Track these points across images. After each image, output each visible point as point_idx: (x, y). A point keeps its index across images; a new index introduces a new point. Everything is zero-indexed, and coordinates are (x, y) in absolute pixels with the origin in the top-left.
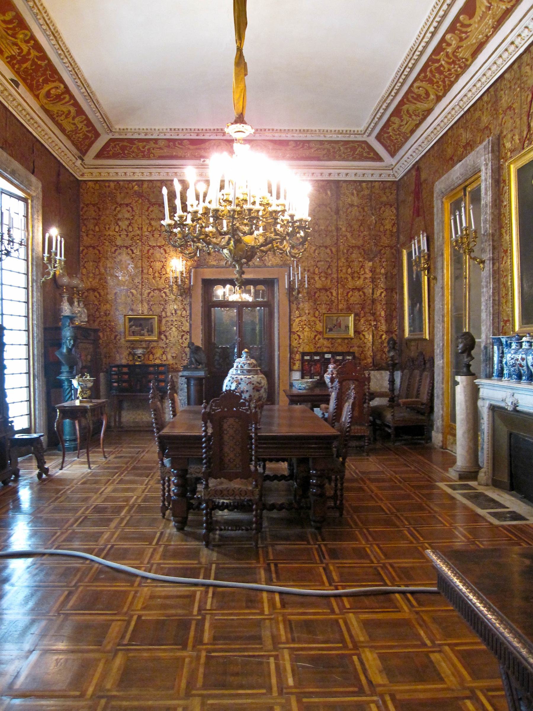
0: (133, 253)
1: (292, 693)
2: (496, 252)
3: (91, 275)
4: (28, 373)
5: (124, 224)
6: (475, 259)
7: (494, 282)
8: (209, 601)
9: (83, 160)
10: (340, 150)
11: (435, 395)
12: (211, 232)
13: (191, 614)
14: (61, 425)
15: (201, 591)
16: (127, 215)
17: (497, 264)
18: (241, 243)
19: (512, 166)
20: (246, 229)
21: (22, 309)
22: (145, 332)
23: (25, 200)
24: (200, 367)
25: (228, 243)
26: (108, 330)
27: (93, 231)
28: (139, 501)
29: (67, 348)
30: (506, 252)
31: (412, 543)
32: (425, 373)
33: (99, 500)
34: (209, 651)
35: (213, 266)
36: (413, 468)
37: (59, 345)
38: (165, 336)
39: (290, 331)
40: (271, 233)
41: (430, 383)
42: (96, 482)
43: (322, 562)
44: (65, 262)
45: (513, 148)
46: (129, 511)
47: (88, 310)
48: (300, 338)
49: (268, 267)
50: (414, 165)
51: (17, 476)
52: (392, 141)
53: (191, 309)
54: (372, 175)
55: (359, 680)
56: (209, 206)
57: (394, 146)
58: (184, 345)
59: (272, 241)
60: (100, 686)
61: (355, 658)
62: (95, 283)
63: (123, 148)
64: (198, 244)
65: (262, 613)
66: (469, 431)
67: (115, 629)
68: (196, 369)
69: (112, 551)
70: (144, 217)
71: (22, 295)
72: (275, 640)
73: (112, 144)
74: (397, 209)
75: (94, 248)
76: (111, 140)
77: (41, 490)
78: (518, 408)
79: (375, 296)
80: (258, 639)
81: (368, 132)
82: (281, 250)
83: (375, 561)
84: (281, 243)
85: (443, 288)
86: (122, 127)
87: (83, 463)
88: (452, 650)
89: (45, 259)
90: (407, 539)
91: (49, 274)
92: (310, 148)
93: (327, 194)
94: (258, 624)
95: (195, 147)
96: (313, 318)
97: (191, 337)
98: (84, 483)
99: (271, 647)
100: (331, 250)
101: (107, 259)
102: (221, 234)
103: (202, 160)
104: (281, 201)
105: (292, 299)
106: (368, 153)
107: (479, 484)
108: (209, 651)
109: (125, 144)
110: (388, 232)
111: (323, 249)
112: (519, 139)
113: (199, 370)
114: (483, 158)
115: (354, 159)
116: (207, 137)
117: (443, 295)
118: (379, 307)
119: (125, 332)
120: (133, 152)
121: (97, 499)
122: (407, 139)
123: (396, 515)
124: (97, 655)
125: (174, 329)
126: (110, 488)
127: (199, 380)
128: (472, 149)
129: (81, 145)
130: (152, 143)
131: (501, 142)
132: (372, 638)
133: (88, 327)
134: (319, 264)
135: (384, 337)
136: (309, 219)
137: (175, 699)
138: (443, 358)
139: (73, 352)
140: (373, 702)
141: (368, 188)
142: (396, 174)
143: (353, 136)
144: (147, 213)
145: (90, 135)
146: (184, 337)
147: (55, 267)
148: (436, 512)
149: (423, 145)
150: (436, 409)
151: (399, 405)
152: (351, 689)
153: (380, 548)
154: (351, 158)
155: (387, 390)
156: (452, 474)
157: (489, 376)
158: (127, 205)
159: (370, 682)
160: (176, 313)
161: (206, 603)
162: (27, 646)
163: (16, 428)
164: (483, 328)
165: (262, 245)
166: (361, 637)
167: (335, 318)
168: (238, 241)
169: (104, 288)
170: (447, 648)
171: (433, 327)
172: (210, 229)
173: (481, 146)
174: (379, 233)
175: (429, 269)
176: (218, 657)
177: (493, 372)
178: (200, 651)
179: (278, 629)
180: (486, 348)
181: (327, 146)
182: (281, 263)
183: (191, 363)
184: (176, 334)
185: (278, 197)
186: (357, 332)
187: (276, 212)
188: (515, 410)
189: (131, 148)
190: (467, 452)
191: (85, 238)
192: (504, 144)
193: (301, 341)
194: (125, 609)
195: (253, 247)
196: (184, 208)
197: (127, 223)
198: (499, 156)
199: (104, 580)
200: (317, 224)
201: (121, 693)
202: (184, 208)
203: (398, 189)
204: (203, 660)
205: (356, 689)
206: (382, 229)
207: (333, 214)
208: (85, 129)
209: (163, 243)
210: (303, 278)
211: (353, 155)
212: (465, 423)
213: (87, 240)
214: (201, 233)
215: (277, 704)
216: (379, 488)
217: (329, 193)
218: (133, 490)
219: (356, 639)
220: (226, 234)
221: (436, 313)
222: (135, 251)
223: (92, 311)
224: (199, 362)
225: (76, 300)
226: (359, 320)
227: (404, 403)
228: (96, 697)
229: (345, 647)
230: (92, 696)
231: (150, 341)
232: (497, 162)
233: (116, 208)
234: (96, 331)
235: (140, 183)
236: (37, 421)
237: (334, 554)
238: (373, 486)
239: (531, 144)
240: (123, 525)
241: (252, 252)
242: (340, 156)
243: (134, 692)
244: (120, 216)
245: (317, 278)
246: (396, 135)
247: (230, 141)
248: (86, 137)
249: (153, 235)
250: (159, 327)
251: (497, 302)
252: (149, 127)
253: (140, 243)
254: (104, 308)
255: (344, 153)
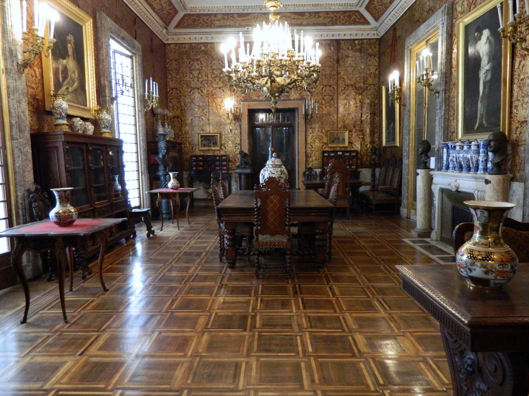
0: (202, 92)
1: (312, 356)
2: (447, 85)
3: (176, 107)
4: (138, 171)
5: (195, 73)
6: (432, 90)
7: (445, 106)
8: (259, 305)
9: (167, 29)
10: (340, 17)
11: (403, 183)
12: (256, 76)
13: (248, 312)
14: (160, 204)
15: (254, 299)
16: (198, 67)
17: (448, 94)
18: (275, 82)
19: (461, 24)
20: (278, 73)
21: (132, 129)
22: (212, 144)
23: (131, 57)
24: (247, 166)
25: (266, 83)
26: (187, 143)
27: (176, 78)
28: (212, 249)
29: (162, 155)
30: (454, 84)
31: (386, 274)
32: (396, 169)
33: (187, 248)
34: (260, 332)
35: (255, 100)
36: (387, 230)
37: (157, 153)
38: (224, 147)
39: (306, 143)
40: (295, 75)
41: (399, 175)
42: (184, 238)
43: (328, 284)
44: (159, 98)
45: (462, 11)
46: (206, 255)
47: (174, 130)
48: (312, 147)
49: (291, 100)
50: (392, 27)
51: (135, 236)
52: (377, 10)
53: (241, 129)
54: (362, 35)
55: (353, 349)
56: (254, 58)
57: (378, 13)
58: (236, 153)
59: (296, 81)
60: (196, 351)
61: (350, 338)
62: (178, 113)
63: (194, 20)
64: (247, 84)
65: (291, 312)
66: (425, 205)
67: (202, 321)
68: (245, 168)
69: (197, 278)
70: (209, 68)
71: (132, 120)
72: (300, 326)
73: (186, 18)
74: (379, 58)
75: (176, 89)
76: (185, 15)
77: (149, 244)
78: (459, 190)
79: (363, 118)
80: (290, 326)
81: (360, 4)
82: (301, 87)
83: (362, 284)
84: (301, 82)
85: (409, 111)
86: (192, 6)
87: (175, 227)
88: (412, 336)
89: (146, 96)
90: (383, 272)
91: (149, 106)
92: (319, 17)
93: (331, 49)
94: (290, 317)
95: (241, 19)
96: (322, 134)
97: (241, 148)
98: (176, 239)
99: (297, 330)
100: (333, 88)
101: (186, 97)
102: (262, 77)
103: (247, 28)
104: (302, 53)
105: (307, 121)
106: (360, 19)
107: (432, 240)
108: (260, 332)
109: (195, 17)
110: (372, 75)
111: (328, 87)
112: (467, 4)
113: (248, 168)
114: (441, 19)
115: (350, 24)
116: (249, 11)
117: (409, 116)
118: (365, 126)
119: (198, 145)
120: (200, 23)
121: (185, 248)
122: (387, 8)
123: (376, 258)
124: (192, 334)
125: (230, 142)
126: (193, 242)
127: (247, 175)
128: (433, 13)
129: (166, 19)
130: (213, 16)
131: (454, 6)
132: (361, 326)
133: (174, 141)
134: (326, 98)
135: (368, 146)
136: (320, 65)
137: (241, 358)
138: (409, 159)
139: (166, 157)
140: (361, 362)
141: (359, 44)
142: (379, 34)
143: (349, 7)
144: (210, 65)
145: (171, 12)
146: (237, 148)
147: (152, 102)
148: (402, 256)
149: (398, 12)
150: (403, 192)
151: (377, 190)
152: (348, 354)
153: (366, 277)
154: (347, 23)
155: (370, 181)
156: (414, 233)
157: (440, 169)
158: (197, 60)
159: (359, 351)
160: (231, 132)
161: (257, 306)
162: (150, 329)
163: (133, 206)
164: (437, 138)
165: (289, 84)
166: (354, 327)
167: (336, 134)
168: (273, 81)
169: (184, 116)
170: (408, 334)
171: (402, 138)
172: (254, 74)
173: (440, 11)
174: (366, 76)
175: (400, 99)
176: (265, 335)
177: (443, 167)
178: (254, 332)
179: (302, 321)
180: (438, 151)
181: (331, 15)
182: (299, 97)
183: (241, 164)
184: (231, 145)
185: (299, 51)
186: (350, 143)
187: (299, 61)
188: (457, 191)
189: (199, 20)
190: (424, 219)
191: (171, 83)
192: (456, 9)
193: (313, 149)
194: (208, 309)
195: (283, 85)
196: (238, 60)
197: (197, 72)
198: (452, 17)
199: (194, 293)
200: (324, 70)
201: (208, 354)
202: (238, 60)
203: (380, 44)
204: (256, 337)
205: (351, 355)
206: (368, 73)
207: (335, 63)
208: (168, 8)
209: (222, 85)
210: (314, 107)
211: (349, 21)
212: (423, 200)
213: (172, 84)
214: (249, 76)
215: (303, 361)
216: (366, 242)
217: (332, 48)
218: (207, 243)
219: (350, 327)
220: (265, 76)
221: (404, 129)
222: (203, 91)
223: (177, 131)
224: (246, 164)
225: (166, 124)
226: (352, 135)
227: (381, 189)
228: (194, 356)
229: (344, 331)
230: (191, 356)
231: (215, 150)
232: (450, 22)
233: (190, 62)
234: (180, 144)
235: (206, 44)
236: (145, 201)
237: (337, 279)
238: (360, 241)
239: (476, 7)
240: (203, 262)
241: (282, 89)
242: (340, 22)
243: (216, 354)
244: (192, 68)
245: (324, 107)
246: (379, 5)
247: (266, 14)
248: (169, 13)
249: (215, 80)
250: (221, 142)
251: (447, 120)
252: (210, 6)
253: (207, 86)
254: (184, 129)
255: (343, 20)
